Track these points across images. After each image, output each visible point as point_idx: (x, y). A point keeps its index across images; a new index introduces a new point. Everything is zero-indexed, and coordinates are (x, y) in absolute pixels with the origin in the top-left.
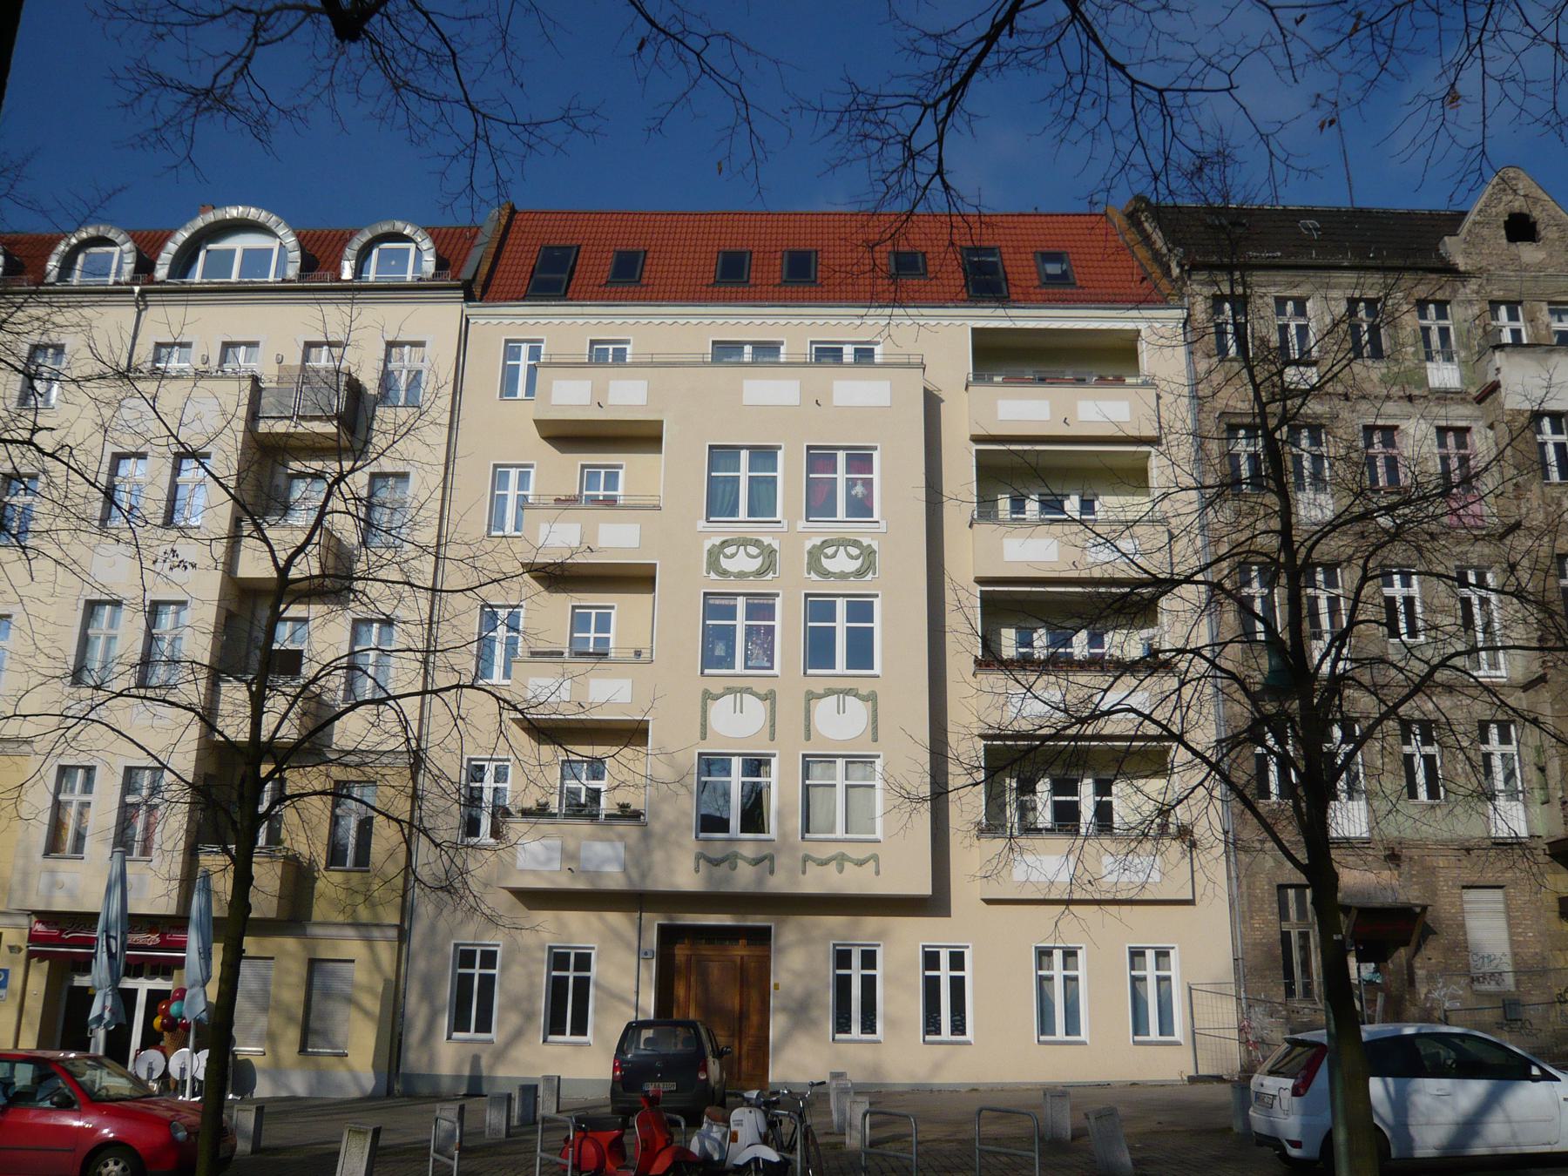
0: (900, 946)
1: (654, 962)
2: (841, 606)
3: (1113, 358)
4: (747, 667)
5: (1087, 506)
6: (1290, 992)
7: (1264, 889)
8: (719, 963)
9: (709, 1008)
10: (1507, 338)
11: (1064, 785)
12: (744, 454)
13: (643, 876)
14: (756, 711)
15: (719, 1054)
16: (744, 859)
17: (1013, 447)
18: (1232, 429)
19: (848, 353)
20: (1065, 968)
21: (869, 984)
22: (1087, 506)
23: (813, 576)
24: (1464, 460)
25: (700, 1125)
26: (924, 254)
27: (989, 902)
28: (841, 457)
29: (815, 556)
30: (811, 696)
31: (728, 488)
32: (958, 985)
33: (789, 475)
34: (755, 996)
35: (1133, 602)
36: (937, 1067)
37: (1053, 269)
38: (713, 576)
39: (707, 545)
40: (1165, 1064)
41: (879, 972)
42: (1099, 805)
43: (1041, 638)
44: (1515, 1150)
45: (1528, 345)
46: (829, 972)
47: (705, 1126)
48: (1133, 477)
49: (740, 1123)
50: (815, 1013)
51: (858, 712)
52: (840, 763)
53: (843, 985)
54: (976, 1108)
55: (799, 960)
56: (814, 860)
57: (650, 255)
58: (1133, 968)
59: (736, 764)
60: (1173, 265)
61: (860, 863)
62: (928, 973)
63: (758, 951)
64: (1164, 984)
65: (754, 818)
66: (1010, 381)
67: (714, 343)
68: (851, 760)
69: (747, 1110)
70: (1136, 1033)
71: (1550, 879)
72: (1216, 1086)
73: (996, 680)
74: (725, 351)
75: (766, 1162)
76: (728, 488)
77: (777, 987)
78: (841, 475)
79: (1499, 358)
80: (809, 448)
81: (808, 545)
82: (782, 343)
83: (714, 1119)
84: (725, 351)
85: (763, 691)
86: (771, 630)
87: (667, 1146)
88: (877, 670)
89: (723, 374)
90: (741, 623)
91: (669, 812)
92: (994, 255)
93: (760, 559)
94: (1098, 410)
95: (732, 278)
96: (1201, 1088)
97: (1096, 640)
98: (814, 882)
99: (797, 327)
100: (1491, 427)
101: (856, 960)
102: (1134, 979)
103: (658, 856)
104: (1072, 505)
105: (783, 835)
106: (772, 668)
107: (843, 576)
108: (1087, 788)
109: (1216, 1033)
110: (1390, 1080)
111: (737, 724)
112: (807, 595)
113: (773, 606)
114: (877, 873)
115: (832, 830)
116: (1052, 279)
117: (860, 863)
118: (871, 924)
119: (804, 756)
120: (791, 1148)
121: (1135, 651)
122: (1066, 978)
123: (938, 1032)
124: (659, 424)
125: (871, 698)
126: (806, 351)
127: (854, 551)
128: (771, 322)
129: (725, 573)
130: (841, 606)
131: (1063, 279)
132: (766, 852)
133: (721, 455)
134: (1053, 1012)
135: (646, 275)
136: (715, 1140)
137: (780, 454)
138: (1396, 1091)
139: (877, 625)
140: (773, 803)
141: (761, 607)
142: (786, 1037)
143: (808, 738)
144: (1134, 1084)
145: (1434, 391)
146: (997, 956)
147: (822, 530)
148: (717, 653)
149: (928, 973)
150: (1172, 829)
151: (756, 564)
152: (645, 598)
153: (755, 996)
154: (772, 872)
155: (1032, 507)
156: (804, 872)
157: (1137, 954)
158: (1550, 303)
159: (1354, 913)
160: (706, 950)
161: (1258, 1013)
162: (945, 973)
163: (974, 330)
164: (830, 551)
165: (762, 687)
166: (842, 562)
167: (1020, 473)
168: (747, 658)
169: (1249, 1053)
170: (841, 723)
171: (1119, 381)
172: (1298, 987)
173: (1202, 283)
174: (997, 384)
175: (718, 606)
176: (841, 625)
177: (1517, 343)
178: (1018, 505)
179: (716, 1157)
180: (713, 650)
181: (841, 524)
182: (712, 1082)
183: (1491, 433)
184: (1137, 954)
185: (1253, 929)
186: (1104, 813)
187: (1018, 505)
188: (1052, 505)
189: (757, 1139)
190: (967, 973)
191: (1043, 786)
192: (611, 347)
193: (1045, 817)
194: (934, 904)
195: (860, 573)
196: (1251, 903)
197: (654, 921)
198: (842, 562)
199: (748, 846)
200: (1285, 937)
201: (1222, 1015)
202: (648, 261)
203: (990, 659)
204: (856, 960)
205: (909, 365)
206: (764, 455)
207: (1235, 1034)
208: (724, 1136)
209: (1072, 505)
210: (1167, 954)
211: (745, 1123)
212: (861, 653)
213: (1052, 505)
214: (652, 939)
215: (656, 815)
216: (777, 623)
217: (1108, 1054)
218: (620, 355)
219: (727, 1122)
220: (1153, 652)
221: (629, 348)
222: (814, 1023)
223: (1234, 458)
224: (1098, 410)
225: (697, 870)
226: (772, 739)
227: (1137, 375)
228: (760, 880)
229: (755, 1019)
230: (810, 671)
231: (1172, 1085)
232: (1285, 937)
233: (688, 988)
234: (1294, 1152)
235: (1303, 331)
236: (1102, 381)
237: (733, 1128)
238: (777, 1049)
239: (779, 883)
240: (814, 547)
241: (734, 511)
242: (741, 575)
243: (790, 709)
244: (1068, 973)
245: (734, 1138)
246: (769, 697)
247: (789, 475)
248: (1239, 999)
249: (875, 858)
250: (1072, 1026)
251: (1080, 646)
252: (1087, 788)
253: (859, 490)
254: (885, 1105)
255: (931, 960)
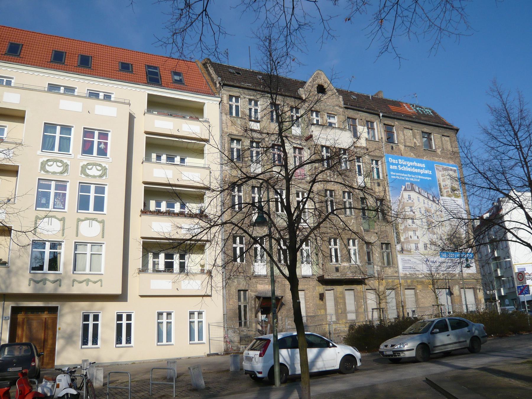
0: (108, 313)
1: (9, 321)
2: (93, 188)
3: (196, 111)
4: (54, 208)
5: (182, 160)
6: (240, 324)
7: (234, 291)
8: (36, 321)
9: (31, 338)
10: (315, 122)
11: (169, 256)
12: (58, 128)
13: (7, 287)
14: (57, 225)
15: (39, 355)
16: (49, 281)
17: (181, 140)
18: (232, 140)
19: (101, 96)
20: (167, 319)
21: (96, 327)
22: (182, 160)
23: (83, 176)
24: (300, 158)
25: (42, 382)
26: (132, 65)
27: (142, 296)
28: (96, 133)
29: (84, 169)
30: (79, 220)
31: (51, 140)
32: (129, 326)
33: (76, 139)
34: (50, 333)
35: (198, 194)
36: (120, 356)
37: (177, 78)
38: (42, 172)
39: (41, 160)
40: (199, 351)
41: (100, 323)
42: (181, 263)
43: (164, 205)
44: (324, 369)
45: (321, 125)
46: (80, 323)
47: (44, 383)
48: (200, 153)
49: (60, 380)
50: (75, 339)
51: (97, 227)
52: (89, 245)
53: (86, 328)
54: (109, 372)
55: (69, 319)
56: (77, 281)
57: (24, 46)
58: (158, 319)
59: (48, 245)
60: (217, 83)
61: (95, 282)
62: (118, 322)
63: (52, 316)
64: (200, 324)
65: (54, 264)
66: (159, 114)
67: (49, 84)
68: (93, 244)
69: (63, 375)
70: (190, 341)
71: (317, 288)
72: (216, 357)
73: (147, 218)
74: (53, 88)
75: (72, 395)
76: (51, 140)
77: (59, 329)
78: (96, 140)
79: (313, 128)
80: (84, 128)
81: (81, 164)
82: (76, 88)
83: (48, 380)
84: (53, 88)
85: (60, 218)
86: (64, 195)
87: (30, 391)
88: (105, 212)
89: (52, 96)
90: (53, 191)
91: (19, 263)
92: (157, 69)
93: (101, 172)
94: (187, 127)
95: (58, 60)
96: (212, 359)
97: (183, 206)
98: (76, 290)
99: (83, 83)
100: (309, 149)
101: (91, 318)
102: (190, 322)
103: (14, 280)
104: (177, 159)
105: (66, 272)
106: (64, 209)
107: (94, 177)
108: (176, 257)
109: (217, 339)
110: (289, 350)
111: (49, 230)
112: (80, 183)
113: (66, 186)
114: (101, 286)
115: (84, 270)
116: (176, 81)
117: (95, 282)
118: (97, 306)
119: (75, 242)
120: (80, 388)
121: (196, 211)
122: (167, 322)
123: (121, 343)
124: (24, 112)
125: (102, 222)
126: (85, 92)
127: (99, 168)
128: (72, 80)
129: (47, 172)
130: (93, 188)
131: (180, 82)
132: (58, 277)
133: (49, 127)
134: (163, 335)
135: (22, 54)
136: (48, 388)
137: (73, 129)
138: (291, 353)
139: (106, 196)
140: (62, 260)
141: (61, 186)
142: (63, 348)
143: (77, 236)
144: (189, 358)
145: (293, 135)
146: (143, 316)
147: (88, 159)
148: (42, 202)
149: (118, 322)
150: (206, 271)
151: (60, 169)
152: (13, 179)
153: (50, 333)
154: (60, 286)
155: (164, 157)
156: (73, 286)
157: (160, 314)
158: (328, 113)
159: (261, 299)
160: (31, 316)
161: (230, 332)
162: (124, 322)
163: (148, 94)
164: (90, 167)
165: (60, 215)
166: (94, 171)
167: (160, 146)
168: (54, 205)
169: (227, 345)
170: (90, 231)
171: (197, 119)
172: (243, 323)
173: (226, 91)
174: (155, 114)
175: (43, 184)
176: (92, 195)
177: (317, 124)
178: (159, 157)
179: (49, 395)
180: (41, 201)
181: (94, 158)
182: (37, 366)
183: (309, 151)
184: (160, 314)
185: (230, 304)
186: (182, 266)
187: (159, 157)
188: (170, 159)
189: (68, 386)
190: (133, 322)
191: (162, 256)
192: (5, 79)
193: (162, 267)
194: (121, 297)
195: (101, 176)
196: (229, 296)
197: (9, 305)
198: (94, 171)
199: (51, 276)
200: (240, 307)
201: (219, 333)
202: (23, 49)
203: (145, 211)
204: (91, 318)
205: (124, 103)
206: (66, 129)
207: (222, 339)
208: (53, 386)
209: (177, 159)
210: (202, 313)
211: (63, 380)
212: (99, 205)
213: (170, 159)
214: (9, 312)
215: (14, 264)
216: (67, 192)
217: (182, 348)
218: (9, 83)
219: (54, 380)
220: (202, 212)
221: (13, 81)
222: (74, 342)
223: (232, 150)
224: (187, 127)
225: (29, 285)
226: (103, 237)
227: (203, 118)
228: (56, 289)
229: (50, 342)
230: (79, 211)
231: (202, 357)
232: (240, 307)
233: (23, 330)
234: (259, 375)
235: (256, 111)
236: (191, 118)
237: (58, 382)
238: (59, 353)
239: (63, 290)
240: (84, 165)
241: (53, 148)
242: (54, 173)
243: (70, 223)
244: (200, 320)
245: (58, 386)
246: (63, 220)
247: (76, 139)
248: (224, 328)
249: (101, 280)
250: (169, 339)
251: (177, 208)
252: (176, 257)
253: (102, 146)
254: (113, 371)
255: (119, 317)
